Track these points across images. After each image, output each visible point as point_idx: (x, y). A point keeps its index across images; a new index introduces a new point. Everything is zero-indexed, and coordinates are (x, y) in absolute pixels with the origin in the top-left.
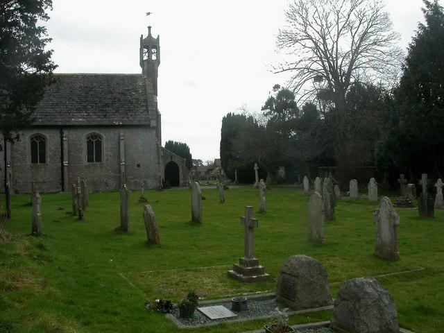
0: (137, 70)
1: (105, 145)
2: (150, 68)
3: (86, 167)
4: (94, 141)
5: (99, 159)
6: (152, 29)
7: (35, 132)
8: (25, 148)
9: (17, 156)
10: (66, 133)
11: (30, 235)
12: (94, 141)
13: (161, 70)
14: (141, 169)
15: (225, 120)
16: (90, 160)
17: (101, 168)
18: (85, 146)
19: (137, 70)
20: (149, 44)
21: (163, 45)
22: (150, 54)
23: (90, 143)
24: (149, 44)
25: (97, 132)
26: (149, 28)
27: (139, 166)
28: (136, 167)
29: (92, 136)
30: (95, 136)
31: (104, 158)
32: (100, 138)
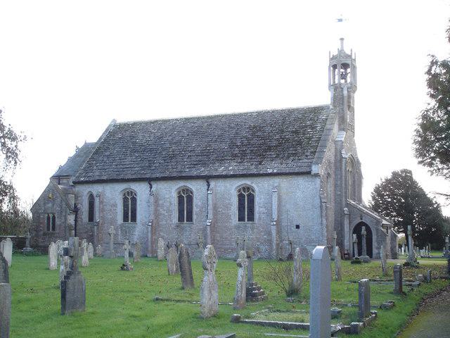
0: (323, 98)
1: (258, 201)
2: (343, 99)
3: (238, 227)
4: (246, 194)
5: (251, 218)
6: (345, 41)
7: (181, 184)
8: (171, 204)
9: (163, 212)
10: (213, 183)
11: (55, 314)
12: (246, 194)
13: (360, 101)
14: (301, 230)
15: (405, 171)
16: (241, 219)
17: (252, 229)
18: (235, 201)
19: (323, 98)
20: (342, 64)
21: (359, 64)
22: (343, 76)
23: (241, 197)
24: (342, 64)
25: (247, 182)
26: (342, 39)
27: (298, 227)
28: (294, 229)
29: (244, 189)
30: (247, 188)
31: (256, 216)
32: (253, 191)
